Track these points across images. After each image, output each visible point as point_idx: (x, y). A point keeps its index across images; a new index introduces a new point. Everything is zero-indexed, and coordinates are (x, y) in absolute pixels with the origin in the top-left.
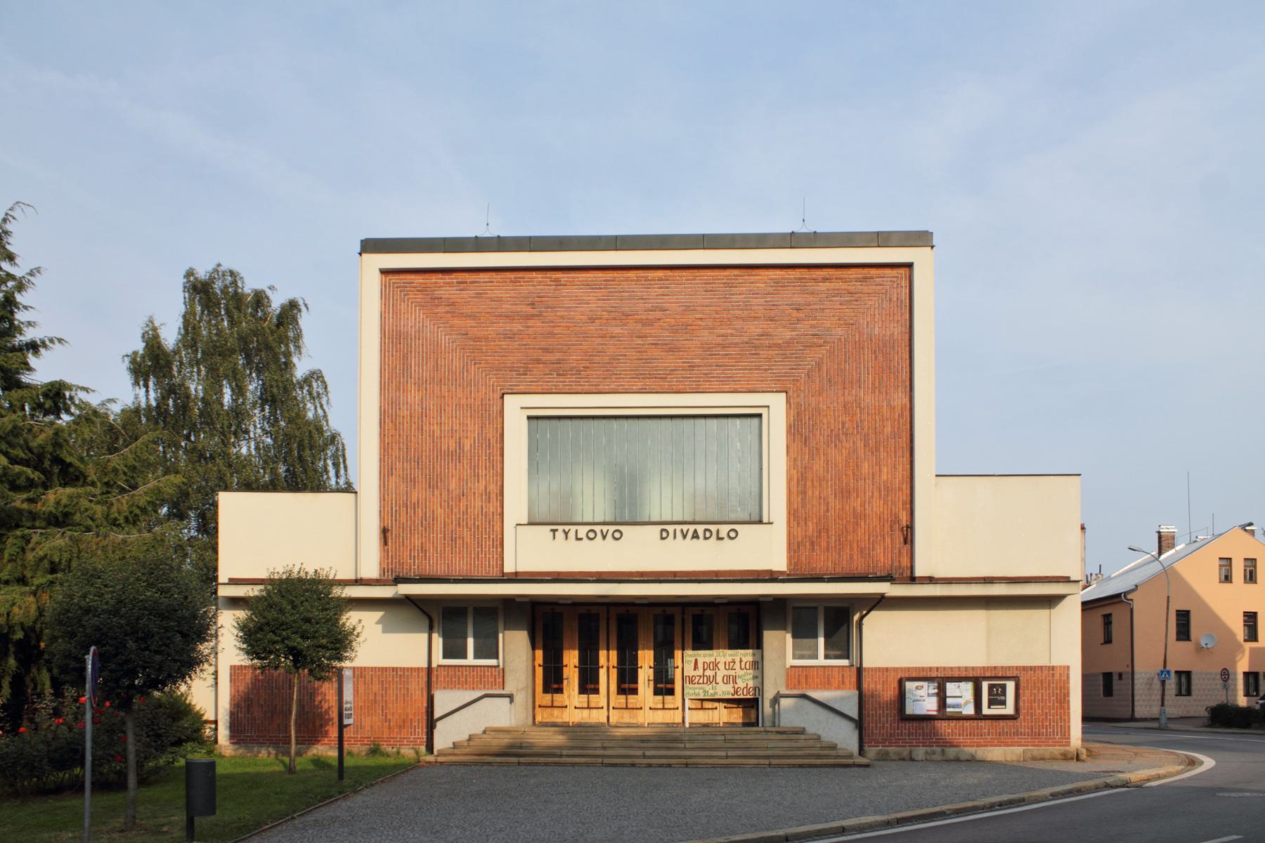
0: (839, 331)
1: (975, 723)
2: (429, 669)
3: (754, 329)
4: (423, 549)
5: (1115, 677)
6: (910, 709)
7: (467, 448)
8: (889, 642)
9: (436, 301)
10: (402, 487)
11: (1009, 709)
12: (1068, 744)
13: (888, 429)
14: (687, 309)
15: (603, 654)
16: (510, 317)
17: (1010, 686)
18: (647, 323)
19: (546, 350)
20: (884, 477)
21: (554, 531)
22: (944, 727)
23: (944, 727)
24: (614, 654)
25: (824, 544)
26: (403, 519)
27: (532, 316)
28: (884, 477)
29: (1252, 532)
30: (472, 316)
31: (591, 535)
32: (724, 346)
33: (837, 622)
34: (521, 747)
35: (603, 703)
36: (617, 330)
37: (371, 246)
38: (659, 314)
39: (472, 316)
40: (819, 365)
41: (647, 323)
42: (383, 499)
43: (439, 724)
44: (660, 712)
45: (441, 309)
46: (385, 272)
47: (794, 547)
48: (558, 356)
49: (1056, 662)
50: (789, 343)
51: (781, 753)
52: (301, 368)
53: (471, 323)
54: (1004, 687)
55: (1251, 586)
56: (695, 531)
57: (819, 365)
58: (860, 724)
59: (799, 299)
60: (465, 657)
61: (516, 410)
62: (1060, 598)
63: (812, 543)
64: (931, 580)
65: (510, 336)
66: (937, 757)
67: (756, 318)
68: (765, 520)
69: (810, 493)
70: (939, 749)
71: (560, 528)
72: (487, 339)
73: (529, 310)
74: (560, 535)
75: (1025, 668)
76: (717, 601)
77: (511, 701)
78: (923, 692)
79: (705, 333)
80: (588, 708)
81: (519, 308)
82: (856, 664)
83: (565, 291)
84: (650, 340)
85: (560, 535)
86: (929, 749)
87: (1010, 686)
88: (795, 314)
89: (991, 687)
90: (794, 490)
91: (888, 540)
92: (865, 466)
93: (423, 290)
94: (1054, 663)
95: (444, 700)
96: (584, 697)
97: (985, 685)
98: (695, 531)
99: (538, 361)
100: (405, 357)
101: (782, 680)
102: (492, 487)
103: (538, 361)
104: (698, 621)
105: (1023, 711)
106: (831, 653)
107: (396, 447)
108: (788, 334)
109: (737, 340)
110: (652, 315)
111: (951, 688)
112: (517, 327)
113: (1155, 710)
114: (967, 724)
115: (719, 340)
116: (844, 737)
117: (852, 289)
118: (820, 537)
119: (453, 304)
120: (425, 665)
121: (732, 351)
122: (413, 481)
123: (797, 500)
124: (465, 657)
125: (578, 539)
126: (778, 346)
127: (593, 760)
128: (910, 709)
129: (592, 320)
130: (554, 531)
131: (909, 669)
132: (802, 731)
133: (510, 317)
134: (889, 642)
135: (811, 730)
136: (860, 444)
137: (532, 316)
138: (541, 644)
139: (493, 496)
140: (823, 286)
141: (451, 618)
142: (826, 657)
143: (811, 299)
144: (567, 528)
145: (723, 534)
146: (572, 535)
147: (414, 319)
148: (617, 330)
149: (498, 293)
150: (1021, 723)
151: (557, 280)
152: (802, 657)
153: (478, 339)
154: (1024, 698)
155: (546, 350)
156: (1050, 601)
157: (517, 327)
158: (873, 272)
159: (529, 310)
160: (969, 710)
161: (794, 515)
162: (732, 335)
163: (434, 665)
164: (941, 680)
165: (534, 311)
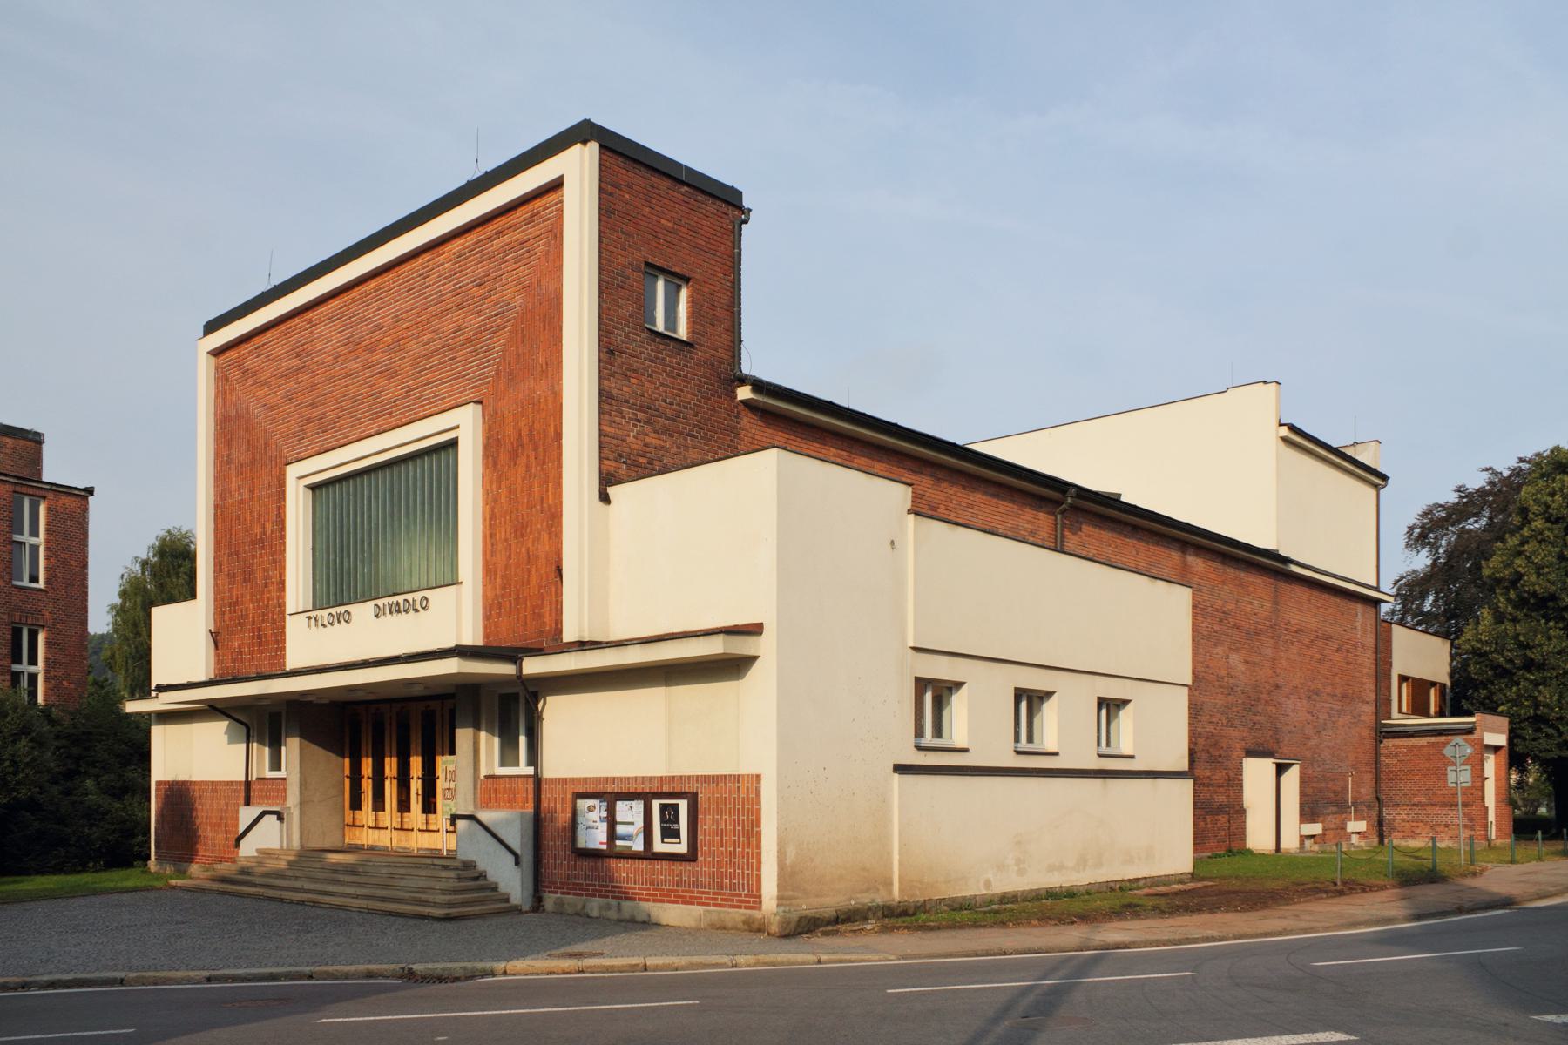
1: (643, 865)
2: (248, 784)
6: (581, 844)
8: (586, 739)
11: (681, 847)
12: (758, 905)
15: (387, 760)
17: (683, 805)
22: (621, 869)
23: (621, 869)
24: (395, 760)
27: (299, 371)
33: (513, 709)
34: (249, 874)
47: (492, 610)
49: (744, 770)
51: (407, 895)
52: (1453, 498)
54: (676, 808)
60: (517, 764)
66: (613, 914)
70: (614, 902)
75: (706, 779)
77: (280, 818)
78: (594, 816)
80: (377, 828)
87: (683, 805)
89: (663, 808)
94: (742, 772)
97: (656, 804)
105: (703, 849)
111: (621, 806)
116: (510, 880)
117: (523, 237)
121: (435, 361)
124: (517, 764)
127: (304, 896)
128: (582, 843)
134: (586, 739)
137: (299, 371)
138: (394, 751)
141: (263, 722)
150: (703, 866)
151: (310, 321)
154: (705, 826)
156: (733, 667)
158: (537, 204)
160: (638, 845)
164: (611, 795)
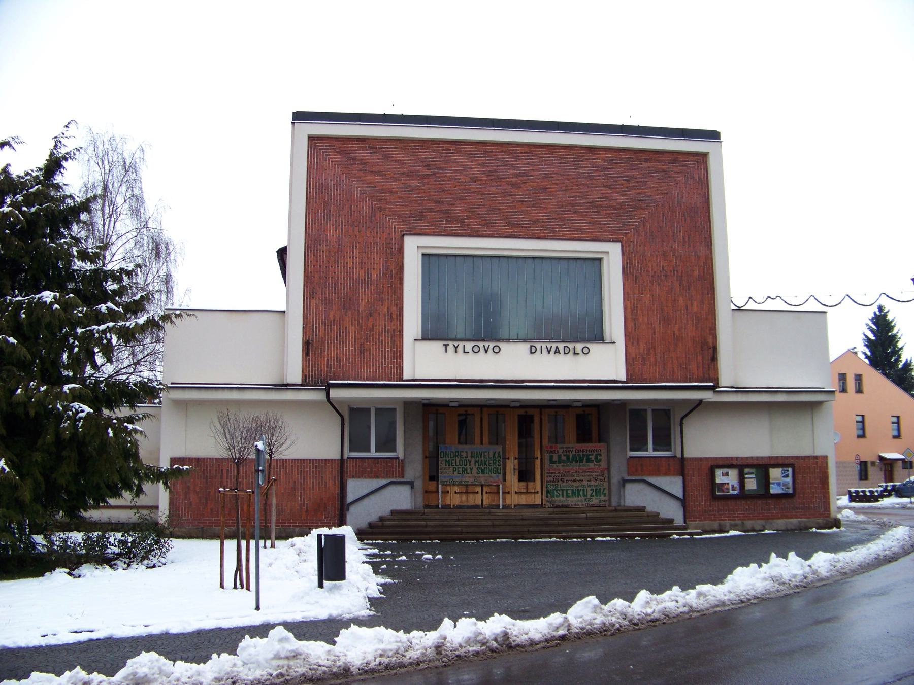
0: (657, 198)
3: (596, 193)
4: (338, 360)
5: (869, 465)
7: (374, 277)
9: (351, 161)
10: (321, 308)
13: (696, 273)
14: (547, 176)
16: (410, 176)
18: (517, 185)
19: (437, 202)
20: (695, 309)
21: (446, 345)
25: (652, 360)
26: (322, 334)
28: (695, 309)
29: (856, 353)
30: (380, 174)
31: (476, 349)
32: (573, 206)
33: (665, 422)
35: (539, 489)
36: (493, 190)
37: (299, 116)
38: (524, 179)
39: (380, 174)
40: (644, 222)
41: (517, 185)
42: (305, 317)
43: (353, 509)
44: (523, 496)
45: (356, 167)
46: (311, 138)
48: (447, 207)
49: (818, 453)
50: (621, 205)
53: (378, 178)
55: (859, 395)
56: (557, 347)
57: (644, 222)
58: (683, 502)
59: (628, 173)
60: (369, 451)
61: (414, 249)
62: (820, 403)
63: (643, 359)
64: (740, 390)
65: (408, 190)
67: (597, 186)
68: (607, 339)
69: (641, 320)
70: (740, 522)
71: (451, 344)
72: (390, 192)
73: (425, 171)
74: (451, 348)
76: (513, 405)
79: (560, 195)
80: (527, 493)
81: (418, 169)
82: (679, 455)
83: (453, 158)
84: (518, 198)
85: (451, 348)
86: (732, 522)
88: (626, 184)
90: (629, 316)
91: (700, 358)
92: (681, 301)
93: (342, 152)
94: (817, 454)
95: (355, 487)
96: (523, 484)
98: (557, 347)
99: (431, 210)
100: (326, 204)
101: (624, 468)
102: (394, 310)
103: (431, 210)
104: (463, 424)
106: (658, 448)
107: (317, 275)
108: (621, 199)
109: (583, 201)
110: (521, 179)
112: (415, 183)
113: (227, 542)
114: (731, 504)
115: (570, 200)
117: (666, 168)
118: (648, 354)
119: (365, 164)
120: (339, 457)
122: (330, 303)
123: (631, 325)
124: (369, 451)
125: (575, 353)
126: (614, 207)
129: (474, 181)
130: (446, 345)
131: (716, 459)
132: (642, 509)
133: (410, 176)
135: (649, 509)
136: (677, 284)
139: (394, 316)
140: (645, 165)
142: (654, 450)
143: (636, 173)
144: (456, 344)
145: (579, 350)
146: (460, 349)
147: (333, 173)
148: (493, 190)
149: (400, 157)
152: (658, 450)
153: (382, 191)
155: (437, 202)
157: (415, 183)
159: (425, 171)
161: (630, 337)
162: (580, 197)
163: (345, 457)
165: (428, 172)
